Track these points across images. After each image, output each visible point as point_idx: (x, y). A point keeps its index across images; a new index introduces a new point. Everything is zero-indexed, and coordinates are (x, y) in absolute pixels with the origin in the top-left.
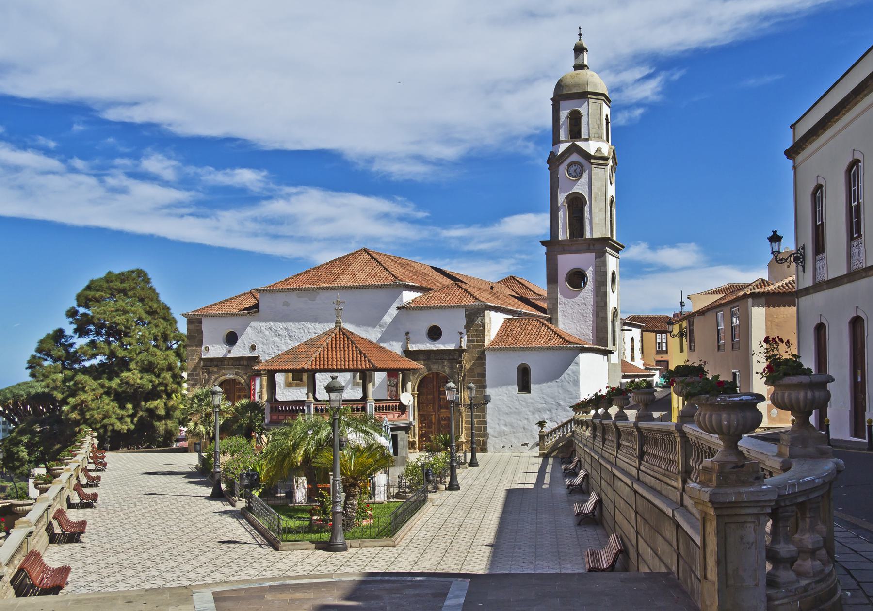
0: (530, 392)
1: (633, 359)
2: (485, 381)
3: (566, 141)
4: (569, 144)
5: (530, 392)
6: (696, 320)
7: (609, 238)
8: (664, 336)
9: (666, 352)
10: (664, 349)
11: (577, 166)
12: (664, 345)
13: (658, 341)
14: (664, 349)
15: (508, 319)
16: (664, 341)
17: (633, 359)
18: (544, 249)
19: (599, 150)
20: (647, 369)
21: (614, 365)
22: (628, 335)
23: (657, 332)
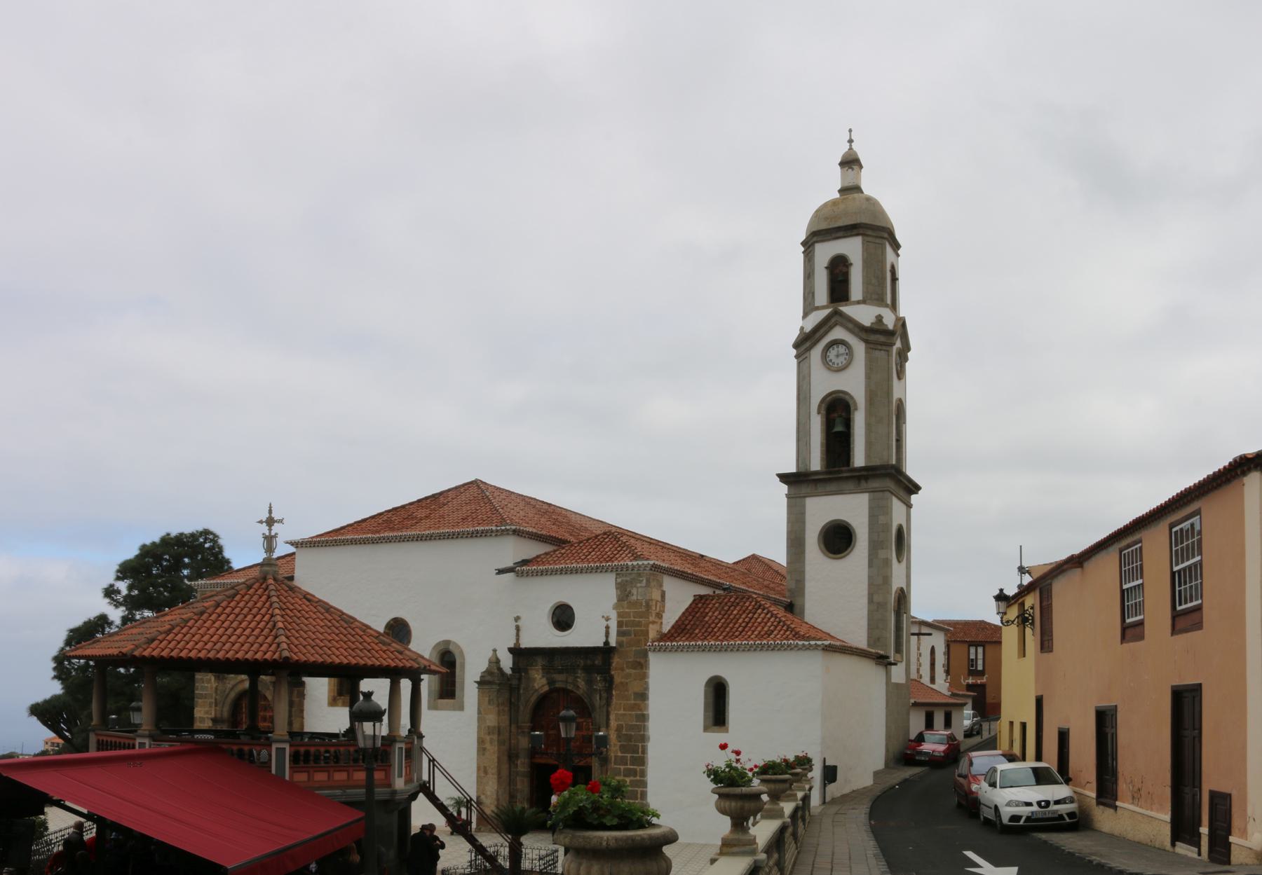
0: (1200, 685)
1: (933, 680)
2: (646, 707)
3: (823, 308)
4: (826, 312)
5: (1200, 685)
6: (1060, 587)
7: (893, 466)
8: (980, 650)
9: (982, 673)
10: (980, 668)
11: (842, 349)
12: (980, 662)
13: (973, 656)
14: (980, 668)
15: (701, 597)
16: (980, 656)
17: (933, 680)
18: (784, 488)
19: (879, 319)
20: (954, 695)
21: (897, 685)
22: (927, 642)
23: (971, 644)
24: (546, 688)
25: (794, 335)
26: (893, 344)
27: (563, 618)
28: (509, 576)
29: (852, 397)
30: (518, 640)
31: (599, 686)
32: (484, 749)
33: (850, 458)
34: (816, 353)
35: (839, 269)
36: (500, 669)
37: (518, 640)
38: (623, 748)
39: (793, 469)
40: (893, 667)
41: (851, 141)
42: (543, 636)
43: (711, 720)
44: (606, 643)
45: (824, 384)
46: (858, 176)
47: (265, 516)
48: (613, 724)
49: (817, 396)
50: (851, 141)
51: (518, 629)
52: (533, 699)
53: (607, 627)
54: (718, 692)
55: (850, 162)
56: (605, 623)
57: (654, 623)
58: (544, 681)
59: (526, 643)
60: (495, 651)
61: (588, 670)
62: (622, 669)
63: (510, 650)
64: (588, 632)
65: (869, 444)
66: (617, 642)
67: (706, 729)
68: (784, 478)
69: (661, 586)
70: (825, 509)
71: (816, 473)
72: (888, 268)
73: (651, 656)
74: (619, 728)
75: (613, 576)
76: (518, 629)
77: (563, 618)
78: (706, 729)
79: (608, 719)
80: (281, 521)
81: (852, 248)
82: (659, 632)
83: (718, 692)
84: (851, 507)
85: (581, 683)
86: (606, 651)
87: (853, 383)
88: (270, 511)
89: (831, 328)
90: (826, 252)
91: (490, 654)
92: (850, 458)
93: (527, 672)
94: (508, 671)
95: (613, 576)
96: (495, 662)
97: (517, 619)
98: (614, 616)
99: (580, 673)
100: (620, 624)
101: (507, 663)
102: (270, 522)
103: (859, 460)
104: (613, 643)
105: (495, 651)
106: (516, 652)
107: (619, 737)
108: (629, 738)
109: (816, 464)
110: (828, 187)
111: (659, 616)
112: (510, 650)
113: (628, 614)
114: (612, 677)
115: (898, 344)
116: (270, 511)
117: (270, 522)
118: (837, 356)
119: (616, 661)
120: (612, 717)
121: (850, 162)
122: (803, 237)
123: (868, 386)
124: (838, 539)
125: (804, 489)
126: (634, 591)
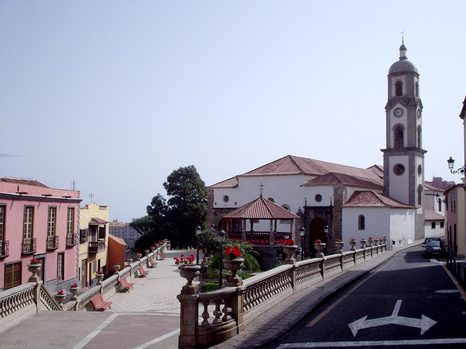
11: (400, 111)
18: (383, 153)
21: (420, 215)
24: (314, 218)
25: (376, 164)
26: (416, 108)
27: (318, 198)
28: (303, 187)
29: (403, 126)
30: (306, 204)
31: (330, 217)
32: (297, 235)
33: (404, 142)
34: (392, 111)
35: (399, 86)
36: (301, 212)
37: (306, 204)
38: (336, 234)
39: (385, 148)
40: (417, 210)
41: (403, 42)
42: (313, 203)
43: (360, 227)
44: (331, 205)
45: (395, 121)
46: (405, 53)
47: (260, 185)
48: (333, 227)
49: (392, 125)
50: (403, 42)
51: (306, 201)
52: (310, 221)
53: (331, 201)
54: (362, 219)
55: (403, 48)
56: (330, 200)
57: (344, 200)
58: (314, 216)
59: (309, 205)
60: (300, 207)
61: (326, 213)
62: (335, 213)
63: (304, 207)
64: (326, 202)
65: (409, 140)
66: (334, 205)
67: (359, 229)
68: (382, 150)
69: (346, 189)
70: (395, 160)
71: (392, 149)
72: (415, 84)
73: (343, 209)
74: (335, 229)
75: (333, 187)
76: (306, 201)
77: (318, 198)
78: (359, 229)
79: (332, 226)
80: (264, 186)
81: (403, 78)
82: (345, 202)
83: (362, 219)
84: (403, 160)
85: (324, 216)
86: (331, 207)
87: (403, 121)
88: (261, 183)
89: (396, 104)
90: (394, 80)
91: (298, 208)
92: (404, 142)
93: (308, 213)
94: (303, 213)
95: (333, 187)
96: (300, 210)
97: (306, 198)
98: (333, 198)
99: (324, 213)
100: (335, 200)
101: (303, 210)
102: (261, 186)
103: (406, 144)
104: (333, 205)
105: (300, 207)
106: (306, 207)
107: (335, 231)
108: (337, 231)
109: (392, 146)
110: (396, 58)
111: (345, 198)
112: (304, 207)
113: (337, 198)
114: (333, 215)
115: (418, 108)
116: (261, 183)
117: (261, 186)
118: (398, 112)
119: (334, 210)
120: (333, 226)
121: (403, 48)
122: (388, 74)
123: (408, 122)
124: (399, 169)
125: (389, 153)
126: (338, 191)
